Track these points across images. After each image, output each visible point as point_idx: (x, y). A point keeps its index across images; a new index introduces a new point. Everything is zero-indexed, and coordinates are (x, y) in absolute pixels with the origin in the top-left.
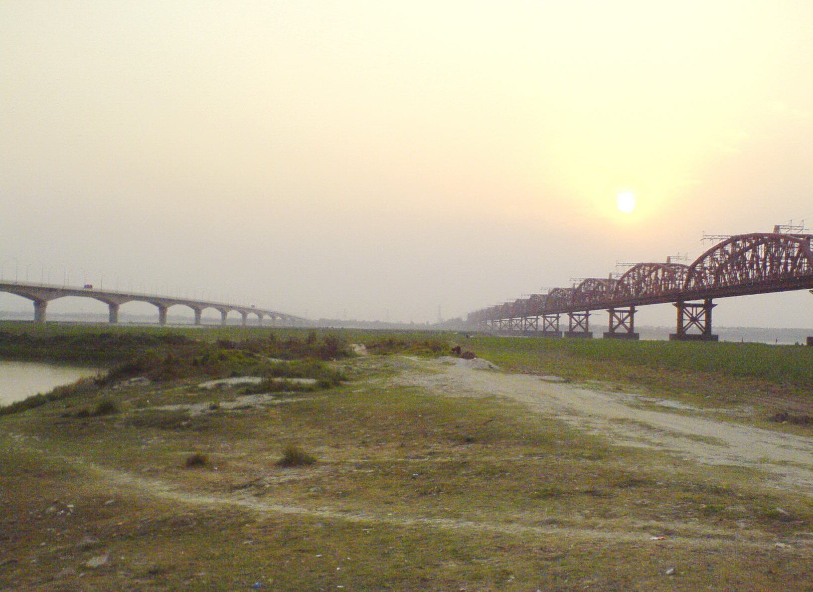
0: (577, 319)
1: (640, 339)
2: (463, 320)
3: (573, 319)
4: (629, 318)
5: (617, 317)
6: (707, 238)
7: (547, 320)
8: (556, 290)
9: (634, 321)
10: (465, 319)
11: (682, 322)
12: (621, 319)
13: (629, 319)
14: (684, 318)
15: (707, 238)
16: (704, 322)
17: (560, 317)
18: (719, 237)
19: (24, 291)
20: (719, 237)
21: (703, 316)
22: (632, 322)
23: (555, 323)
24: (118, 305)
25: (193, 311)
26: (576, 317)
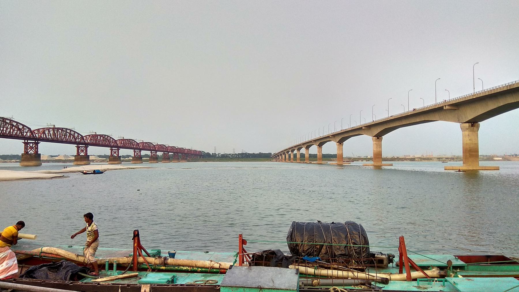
26: (153, 153)
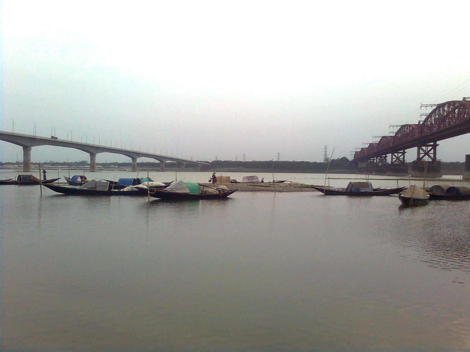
0: (397, 156)
1: (132, 162)
2: (350, 160)
3: (393, 156)
4: (433, 150)
5: (423, 150)
6: (423, 106)
7: (423, 154)
8: (403, 127)
9: (10, 186)
10: (351, 158)
11: (419, 155)
12: (427, 151)
13: (432, 151)
14: (177, 172)
15: (423, 106)
16: (433, 155)
17: (405, 152)
18: (430, 106)
19: (6, 138)
20: (430, 106)
21: (432, 151)
22: (435, 153)
23: (402, 157)
24: (136, 158)
25: (21, 148)
